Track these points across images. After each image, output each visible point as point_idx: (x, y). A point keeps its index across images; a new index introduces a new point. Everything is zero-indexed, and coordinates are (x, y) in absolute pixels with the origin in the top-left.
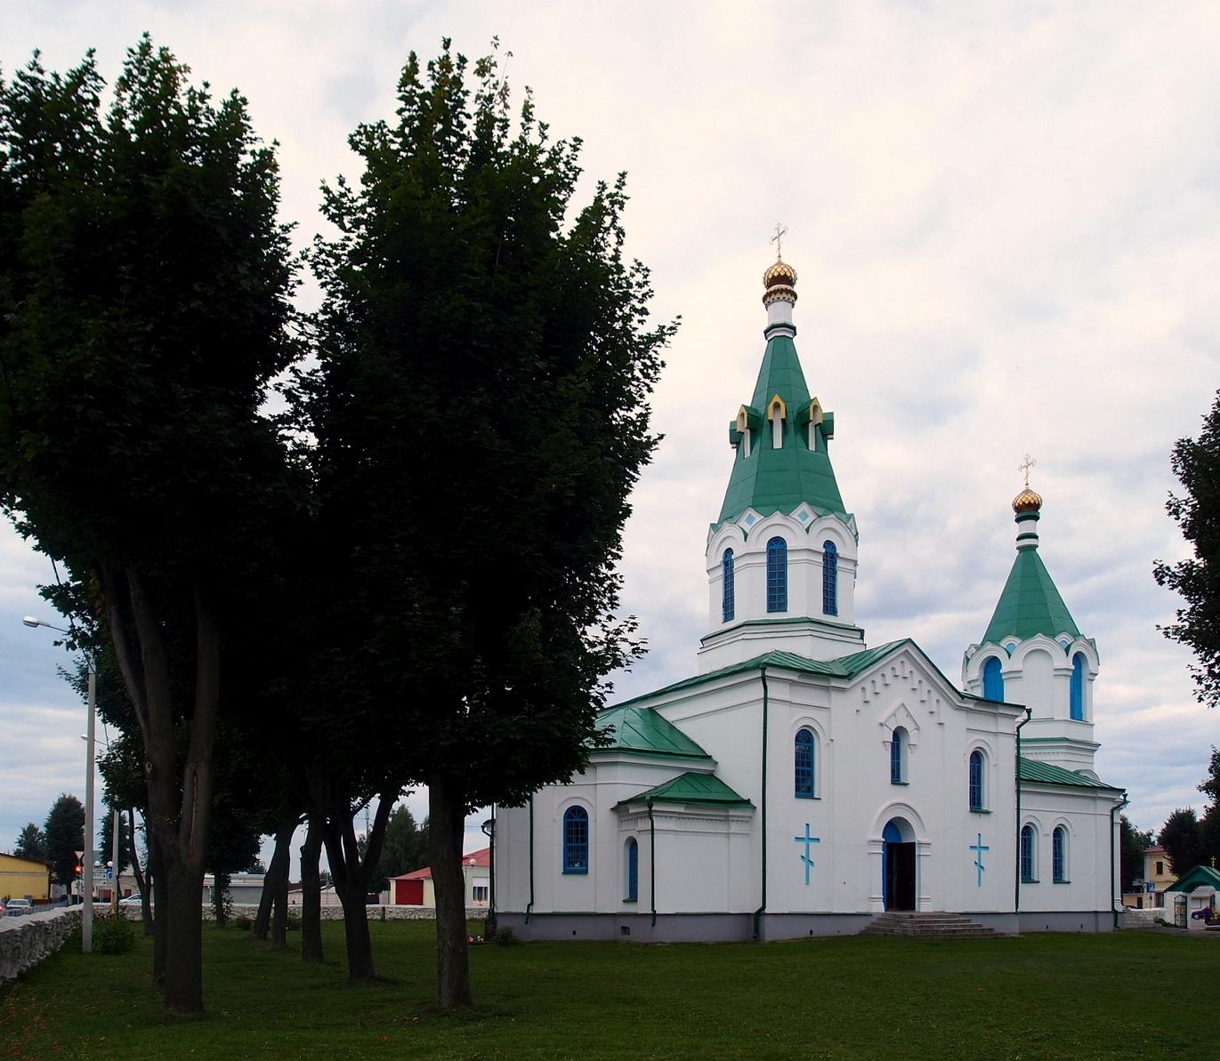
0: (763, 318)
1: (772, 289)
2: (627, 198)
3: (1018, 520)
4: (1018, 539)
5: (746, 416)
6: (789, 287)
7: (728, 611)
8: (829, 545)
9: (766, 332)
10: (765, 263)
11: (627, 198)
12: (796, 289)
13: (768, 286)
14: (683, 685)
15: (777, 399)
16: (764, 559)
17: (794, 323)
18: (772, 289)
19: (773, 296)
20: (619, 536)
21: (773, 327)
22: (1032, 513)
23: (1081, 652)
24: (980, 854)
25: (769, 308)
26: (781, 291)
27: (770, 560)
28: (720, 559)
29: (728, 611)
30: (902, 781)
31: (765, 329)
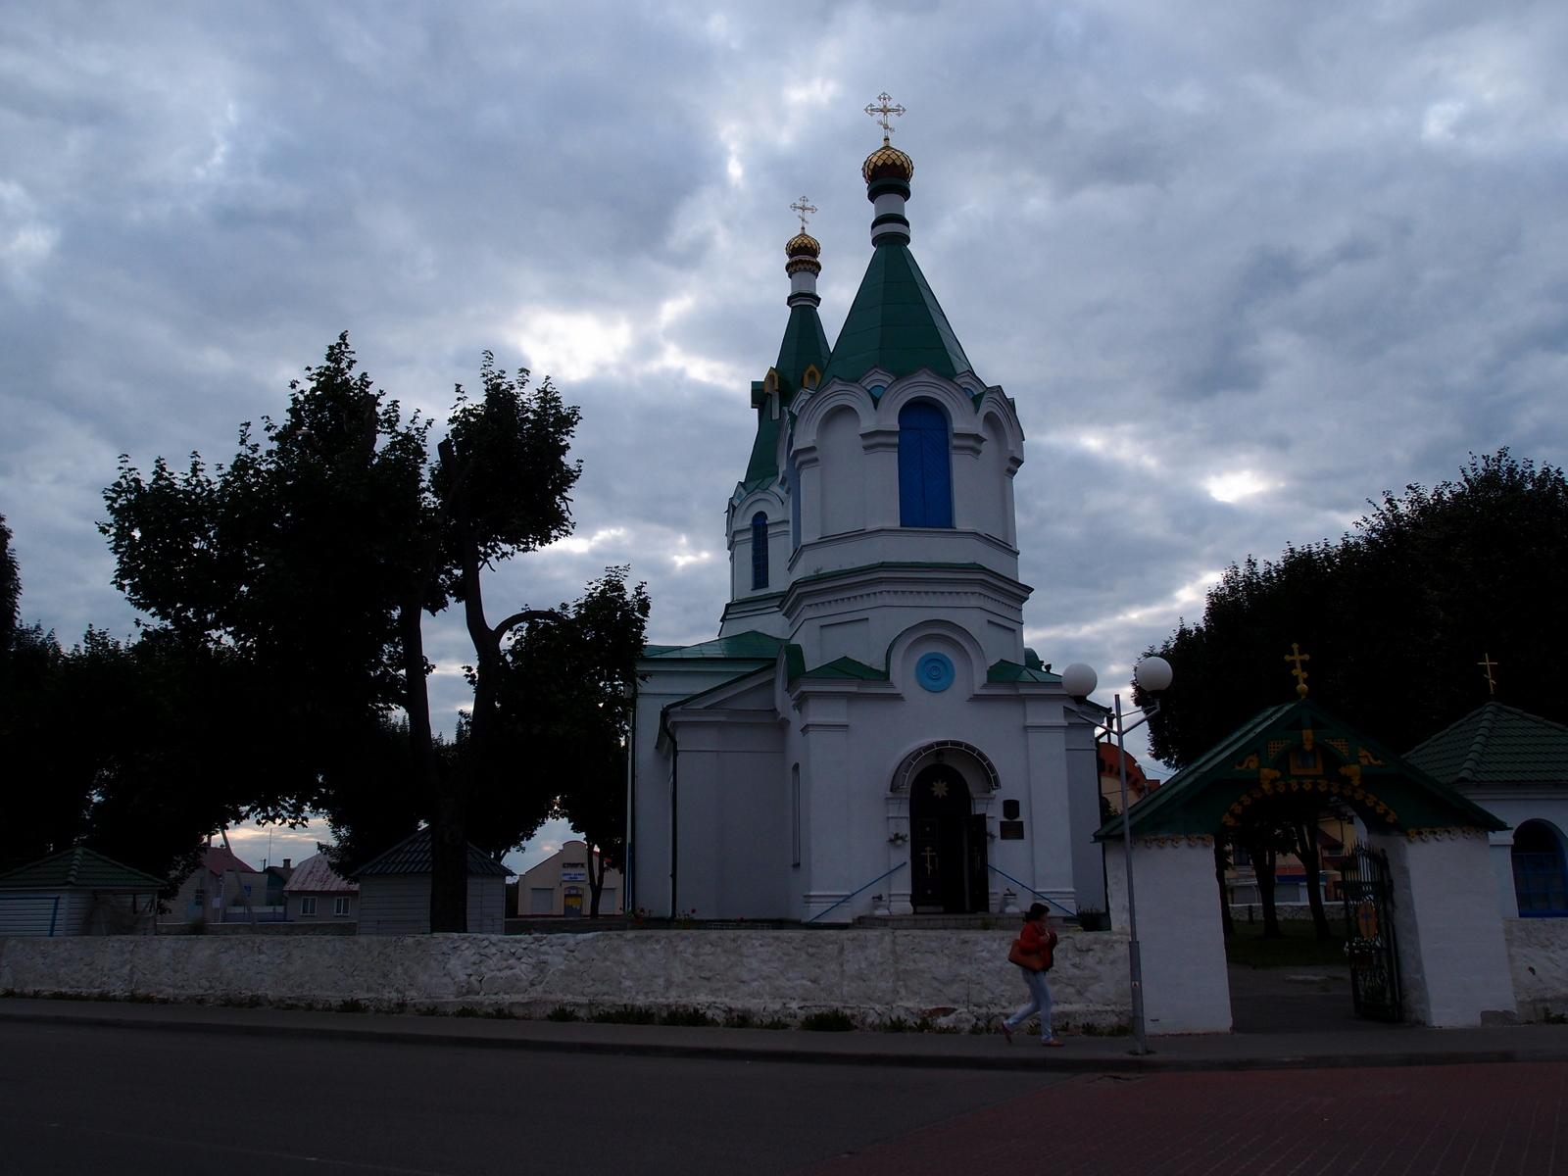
1: (796, 258)
4: (874, 226)
7: (761, 577)
8: (760, 517)
16: (750, 535)
18: (796, 258)
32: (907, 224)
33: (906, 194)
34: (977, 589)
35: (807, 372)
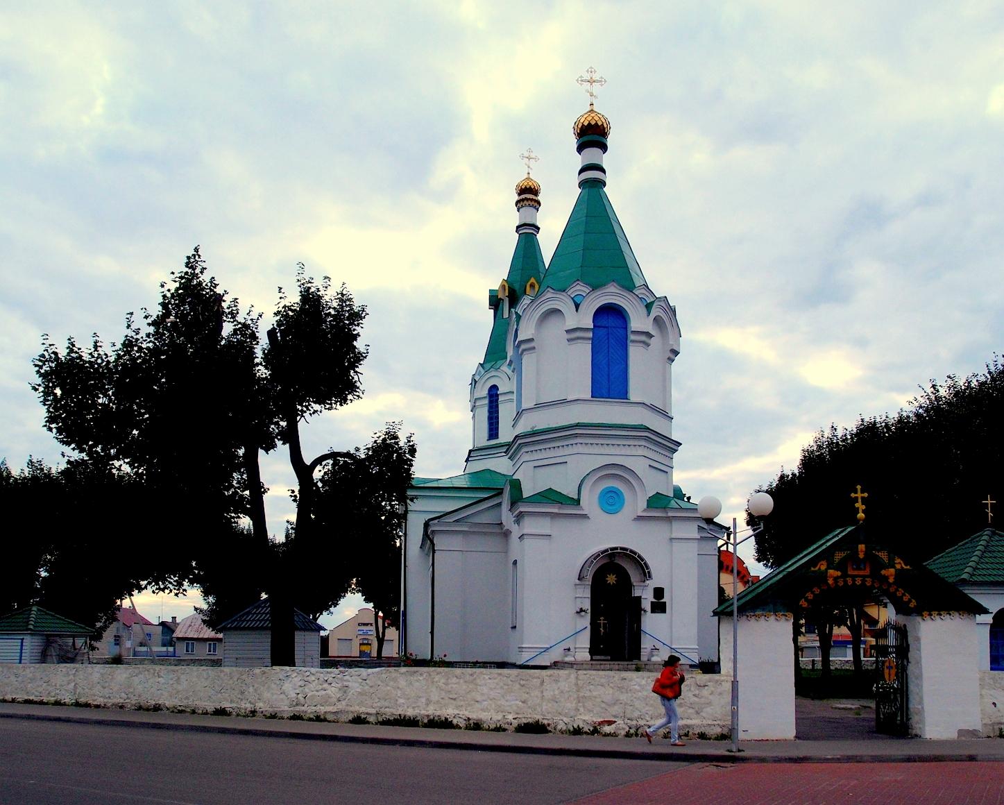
0: (515, 218)
1: (523, 196)
2: (639, 518)
3: (580, 149)
4: (581, 172)
5: (507, 288)
6: (534, 197)
7: (493, 432)
9: (518, 227)
10: (519, 178)
11: (639, 518)
12: (540, 198)
13: (519, 195)
14: (600, 428)
15: (533, 280)
17: (539, 224)
18: (523, 196)
19: (525, 202)
20: (276, 444)
21: (525, 225)
22: (595, 138)
23: (658, 316)
24: (485, 397)
25: (521, 210)
26: (527, 199)
27: (491, 402)
28: (485, 392)
29: (493, 432)
30: (716, 661)
31: (517, 225)
32: (603, 171)
33: (604, 148)
34: (643, 443)
35: (529, 283)
